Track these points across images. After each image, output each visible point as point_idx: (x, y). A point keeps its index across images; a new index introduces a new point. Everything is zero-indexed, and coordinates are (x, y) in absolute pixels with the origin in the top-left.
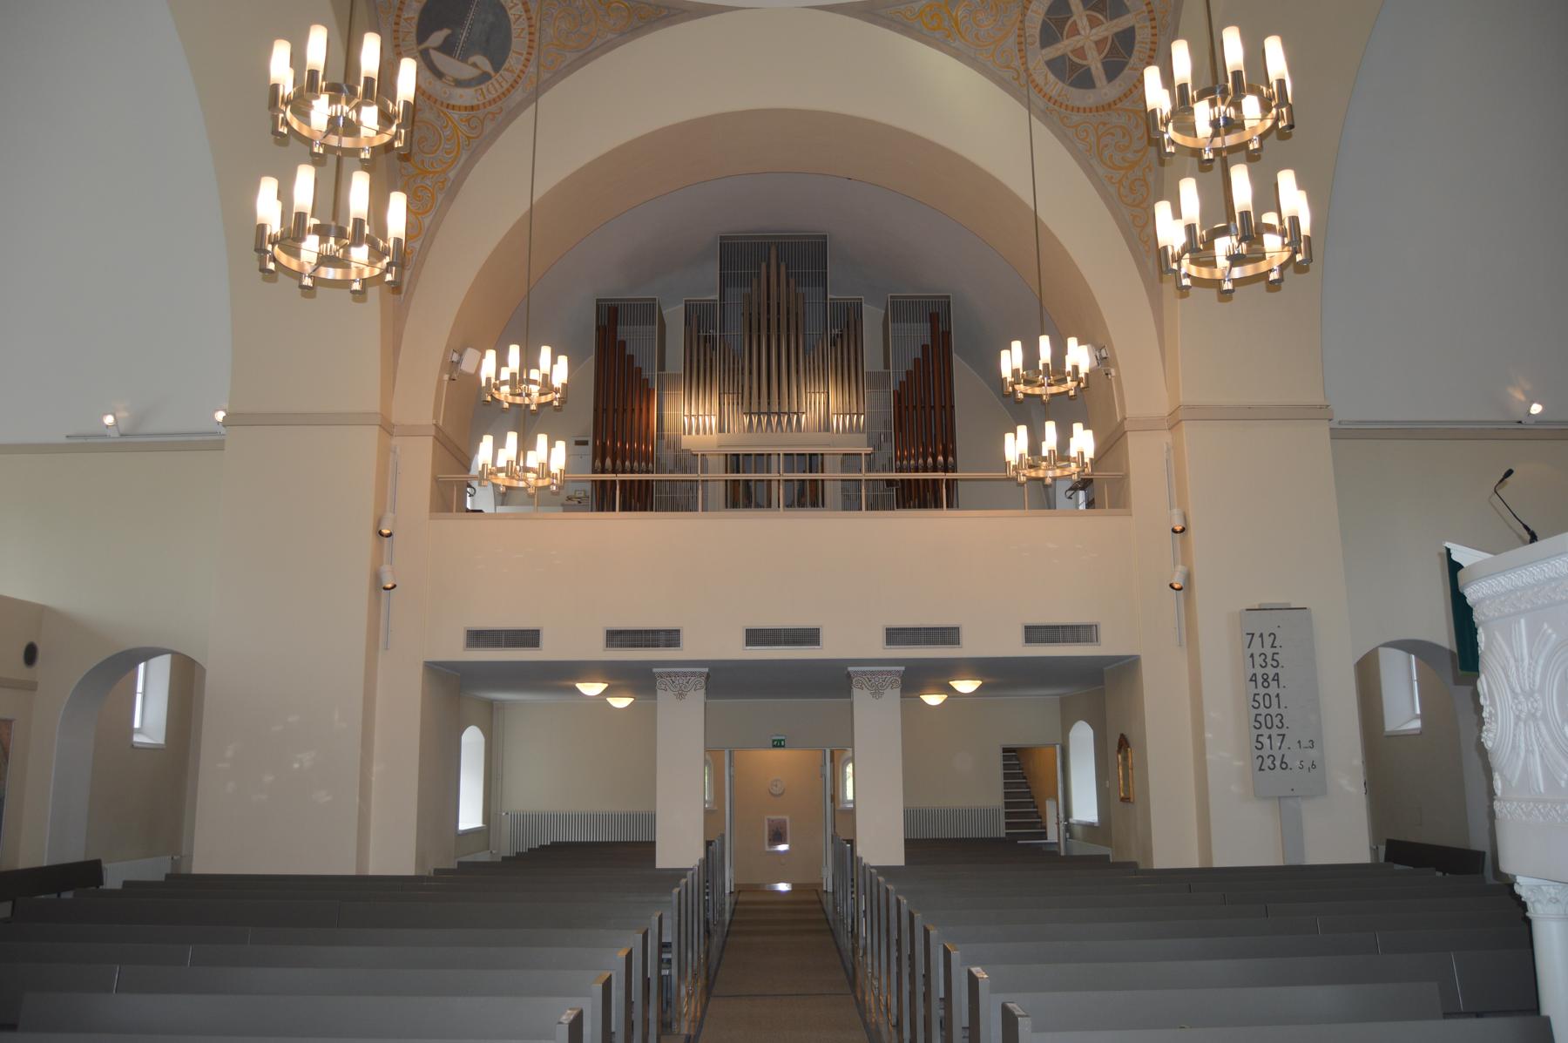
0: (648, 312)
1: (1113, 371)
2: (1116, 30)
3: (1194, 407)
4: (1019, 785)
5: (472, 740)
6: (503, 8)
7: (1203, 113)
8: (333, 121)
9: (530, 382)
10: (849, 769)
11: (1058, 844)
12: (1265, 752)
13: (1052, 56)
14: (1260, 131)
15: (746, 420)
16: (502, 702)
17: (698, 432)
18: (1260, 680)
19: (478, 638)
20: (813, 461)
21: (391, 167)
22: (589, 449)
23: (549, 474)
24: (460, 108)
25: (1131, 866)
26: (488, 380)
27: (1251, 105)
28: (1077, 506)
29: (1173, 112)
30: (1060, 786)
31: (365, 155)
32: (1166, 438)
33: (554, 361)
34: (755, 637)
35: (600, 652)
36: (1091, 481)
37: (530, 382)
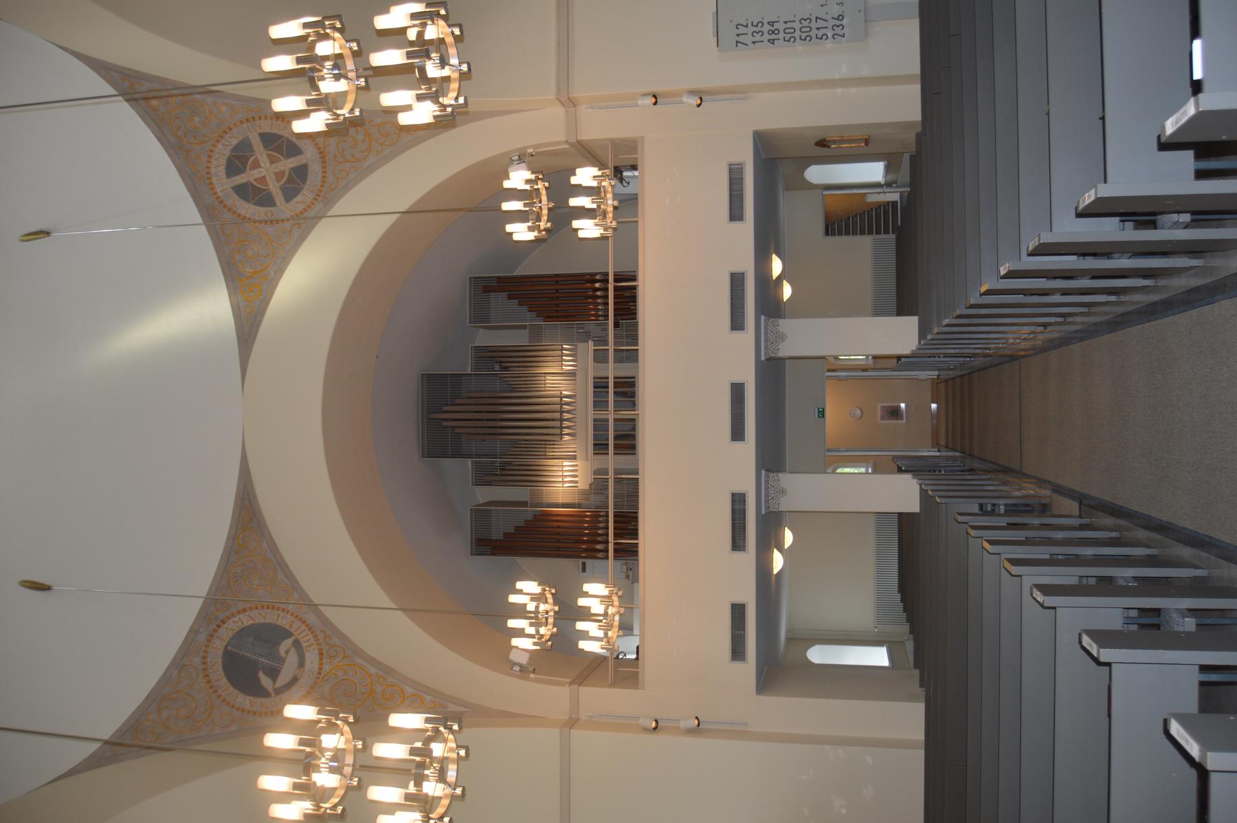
0: (481, 515)
1: (530, 151)
2: (274, 192)
3: (558, 88)
4: (855, 223)
5: (818, 655)
6: (242, 630)
7: (328, 86)
8: (332, 770)
9: (537, 612)
10: (863, 470)
11: (901, 193)
13: (282, 199)
14: (343, 42)
15: (566, 438)
16: (788, 631)
17: (575, 476)
18: (773, 36)
19: (738, 652)
20: (600, 385)
21: (370, 723)
22: (589, 562)
23: (609, 597)
24: (321, 664)
25: (920, 138)
26: (535, 644)
27: (323, 48)
28: (635, 177)
29: (328, 110)
30: (855, 191)
31: (359, 745)
32: (583, 110)
33: (520, 592)
34: (737, 433)
35: (748, 558)
36: (616, 168)
37: (537, 612)
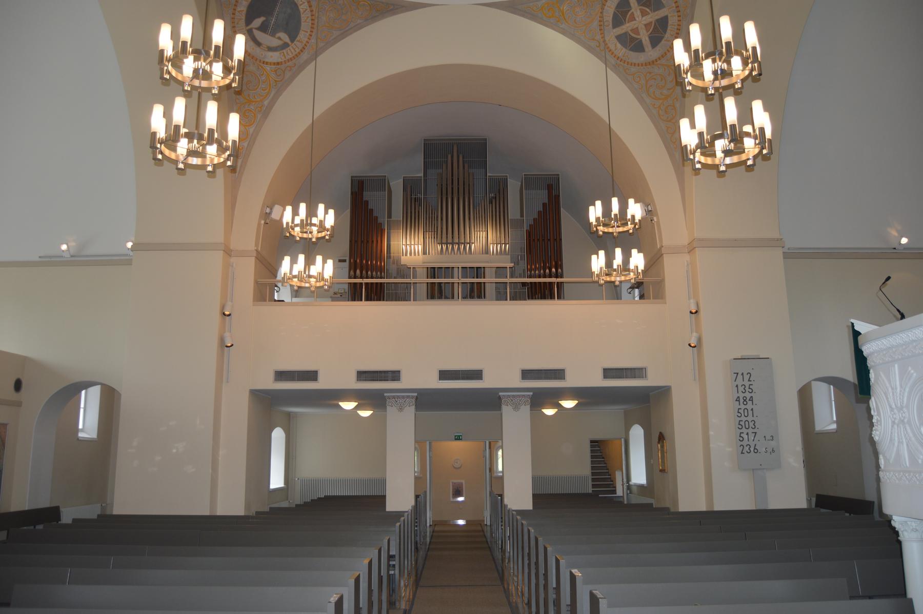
0: (381, 183)
1: (655, 219)
2: (657, 17)
3: (703, 240)
4: (600, 462)
5: (278, 436)
6: (296, 5)
7: (708, 67)
8: (196, 71)
9: (312, 225)
11: (623, 497)
12: (745, 443)
13: (619, 33)
14: (742, 77)
15: (439, 247)
16: (296, 413)
17: (411, 254)
18: (742, 400)
19: (281, 375)
20: (478, 272)
21: (230, 98)
22: (347, 264)
23: (323, 279)
24: (271, 64)
25: (666, 510)
26: (287, 223)
27: (736, 62)
28: (634, 298)
29: (691, 66)
30: (624, 462)
31: (215, 91)
32: (686, 258)
33: (326, 212)
34: (445, 375)
35: (353, 384)
36: (642, 283)
37: (312, 225)
